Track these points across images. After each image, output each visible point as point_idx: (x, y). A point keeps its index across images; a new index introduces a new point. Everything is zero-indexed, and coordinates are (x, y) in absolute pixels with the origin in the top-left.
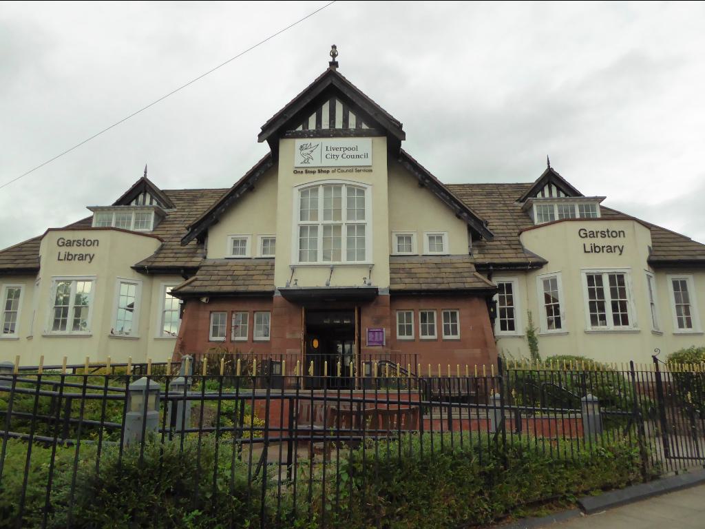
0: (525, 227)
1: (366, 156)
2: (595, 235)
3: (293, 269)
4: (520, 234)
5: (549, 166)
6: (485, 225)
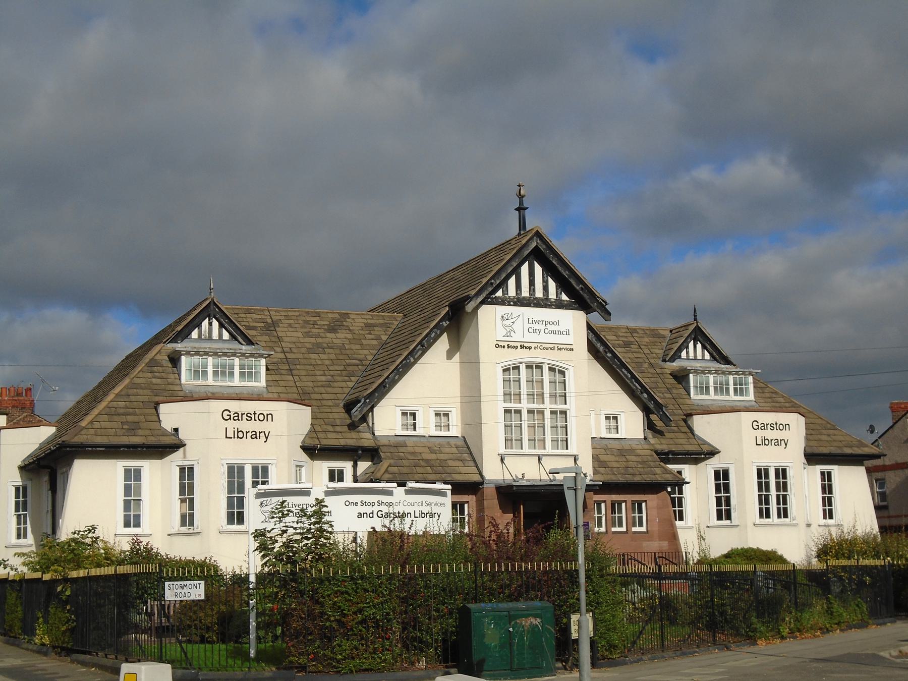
1: (568, 333)
2: (240, 418)
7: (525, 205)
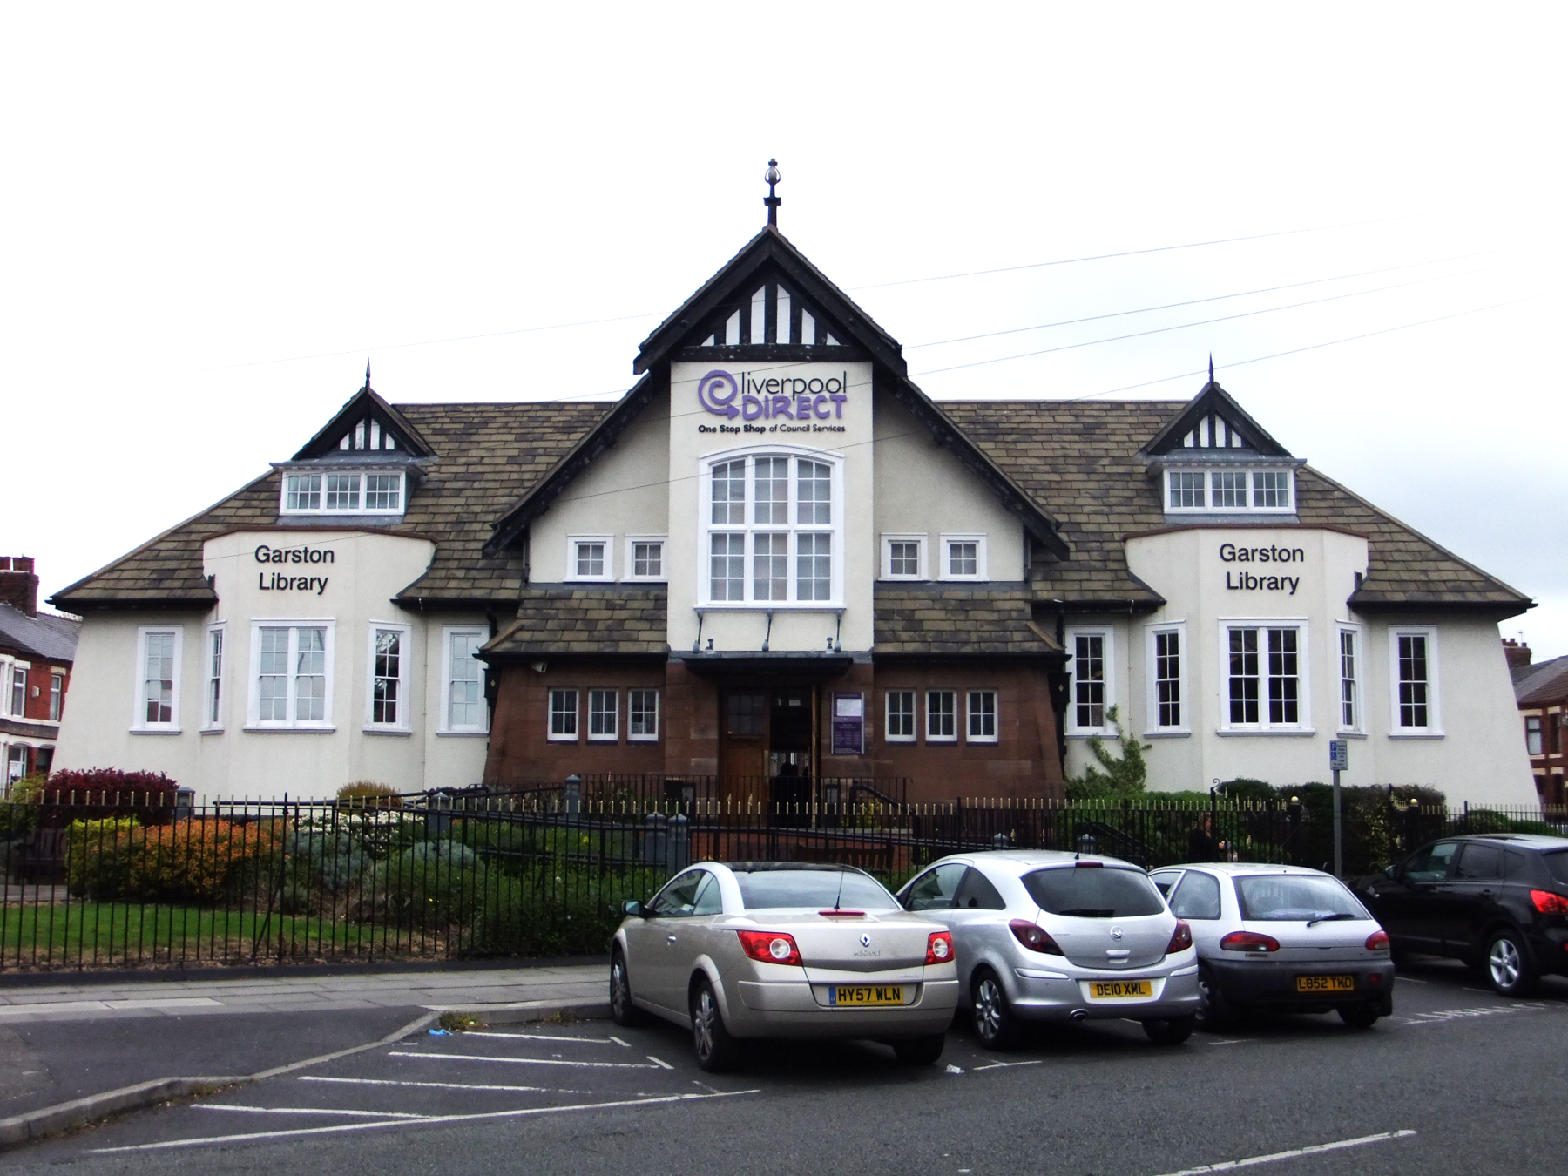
0: (1133, 528)
3: (701, 615)
4: (1125, 540)
5: (1212, 378)
6: (1054, 528)
7: (777, 195)
